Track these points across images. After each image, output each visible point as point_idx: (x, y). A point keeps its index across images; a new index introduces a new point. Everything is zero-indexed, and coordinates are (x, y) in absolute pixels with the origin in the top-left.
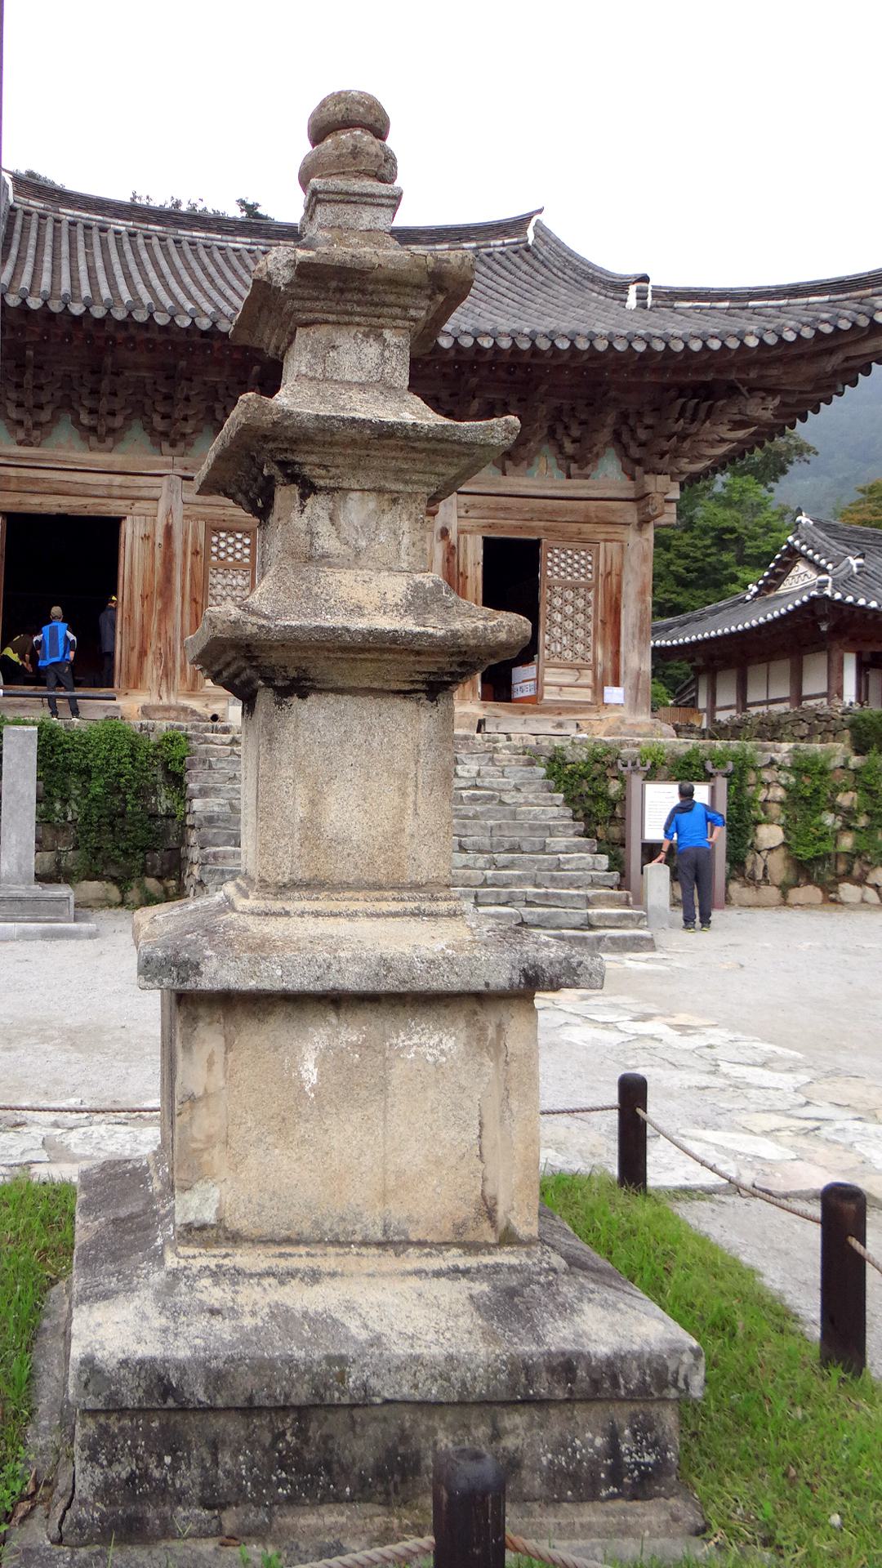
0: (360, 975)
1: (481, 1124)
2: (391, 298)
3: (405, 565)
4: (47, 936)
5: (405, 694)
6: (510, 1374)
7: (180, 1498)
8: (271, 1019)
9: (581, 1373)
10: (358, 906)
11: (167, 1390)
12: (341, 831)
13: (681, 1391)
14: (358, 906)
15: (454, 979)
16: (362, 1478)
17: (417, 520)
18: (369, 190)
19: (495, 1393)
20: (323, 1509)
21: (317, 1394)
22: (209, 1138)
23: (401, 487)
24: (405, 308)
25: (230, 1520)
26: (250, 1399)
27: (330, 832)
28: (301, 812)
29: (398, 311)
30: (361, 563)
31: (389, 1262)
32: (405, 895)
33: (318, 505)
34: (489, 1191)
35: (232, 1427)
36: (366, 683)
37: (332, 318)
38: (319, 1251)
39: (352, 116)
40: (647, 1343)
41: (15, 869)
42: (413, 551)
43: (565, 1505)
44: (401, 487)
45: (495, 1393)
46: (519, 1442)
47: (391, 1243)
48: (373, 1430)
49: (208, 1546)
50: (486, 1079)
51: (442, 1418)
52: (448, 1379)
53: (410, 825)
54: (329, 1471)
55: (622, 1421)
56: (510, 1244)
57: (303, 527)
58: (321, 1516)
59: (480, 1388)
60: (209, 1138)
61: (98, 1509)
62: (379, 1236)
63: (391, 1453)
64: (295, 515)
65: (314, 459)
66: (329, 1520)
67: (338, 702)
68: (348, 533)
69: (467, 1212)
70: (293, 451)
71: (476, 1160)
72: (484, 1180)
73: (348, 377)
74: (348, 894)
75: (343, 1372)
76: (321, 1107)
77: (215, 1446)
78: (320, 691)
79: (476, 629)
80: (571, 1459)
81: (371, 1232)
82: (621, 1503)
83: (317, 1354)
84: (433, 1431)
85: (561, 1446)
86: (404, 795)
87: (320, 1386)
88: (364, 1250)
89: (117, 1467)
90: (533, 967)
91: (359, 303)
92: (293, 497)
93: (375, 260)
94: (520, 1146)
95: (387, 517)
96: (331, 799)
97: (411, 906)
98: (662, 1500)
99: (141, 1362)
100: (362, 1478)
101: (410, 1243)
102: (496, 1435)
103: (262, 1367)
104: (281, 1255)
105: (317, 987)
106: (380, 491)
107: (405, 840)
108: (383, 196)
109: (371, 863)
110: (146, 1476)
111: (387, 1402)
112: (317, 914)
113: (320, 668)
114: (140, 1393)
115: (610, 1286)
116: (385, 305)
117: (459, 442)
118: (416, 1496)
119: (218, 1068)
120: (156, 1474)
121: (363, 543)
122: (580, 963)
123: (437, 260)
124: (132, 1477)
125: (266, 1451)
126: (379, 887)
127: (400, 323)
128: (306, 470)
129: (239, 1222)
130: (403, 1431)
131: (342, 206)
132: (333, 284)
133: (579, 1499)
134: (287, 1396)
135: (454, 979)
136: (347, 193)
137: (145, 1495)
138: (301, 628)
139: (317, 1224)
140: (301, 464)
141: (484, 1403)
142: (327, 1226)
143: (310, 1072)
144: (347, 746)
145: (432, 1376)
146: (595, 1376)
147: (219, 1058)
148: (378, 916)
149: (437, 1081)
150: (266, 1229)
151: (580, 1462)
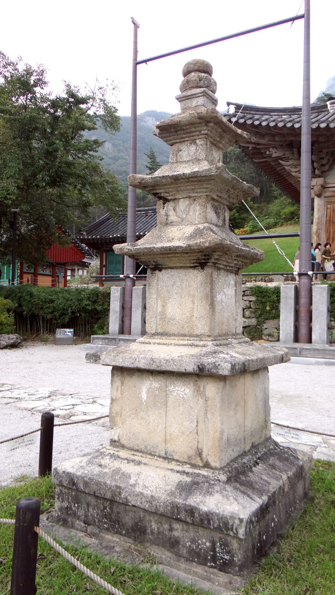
0: (145, 363)
1: (197, 421)
2: (193, 129)
3: (197, 222)
4: (326, 364)
5: (194, 267)
6: (171, 508)
7: (78, 518)
8: (134, 377)
9: (196, 515)
10: (173, 342)
11: (74, 484)
12: (180, 314)
13: (235, 534)
14: (173, 342)
15: (175, 367)
16: (128, 530)
17: (202, 205)
18: (193, 93)
19: (166, 513)
20: (115, 535)
21: (113, 496)
22: (117, 413)
23: (196, 195)
24: (200, 131)
25: (90, 529)
26: (94, 492)
27: (169, 316)
28: (160, 309)
29: (198, 133)
30: (184, 223)
31: (165, 464)
32: (192, 339)
33: (170, 206)
34: (200, 446)
35: (92, 500)
36: (178, 265)
37: (178, 141)
38: (145, 456)
39: (190, 69)
40: (224, 511)
41: (318, 339)
42: (200, 216)
43: (194, 563)
44: (196, 195)
45: (166, 513)
46: (179, 534)
47: (167, 458)
48: (131, 514)
49: (82, 534)
50: (200, 405)
51: (154, 518)
52: (151, 504)
53: (196, 314)
54: (119, 524)
55: (217, 539)
56: (208, 468)
57: (164, 214)
58: (113, 537)
59: (162, 510)
60: (117, 413)
61: (58, 513)
62: (164, 455)
63: (136, 524)
64: (161, 210)
65: (162, 191)
66: (114, 539)
67: (171, 272)
68: (180, 213)
69: (192, 452)
70: (155, 190)
71: (196, 435)
72: (198, 442)
73: (185, 160)
74: (173, 338)
75: (120, 492)
76: (147, 408)
77: (88, 505)
78: (165, 268)
79: (196, 243)
80: (197, 547)
81: (161, 453)
82: (215, 571)
83: (113, 484)
84: (151, 521)
85: (193, 541)
86: (194, 303)
87: (114, 495)
88: (158, 459)
89: (64, 503)
90: (201, 365)
91: (184, 134)
92: (160, 204)
93: (178, 119)
94: (212, 432)
95: (192, 206)
96: (169, 305)
97: (190, 342)
98: (231, 575)
99: (68, 473)
100: (128, 530)
101: (174, 460)
102: (171, 529)
103: (98, 483)
104: (133, 455)
105: (132, 366)
106: (189, 197)
107: (194, 319)
108: (198, 94)
109: (183, 327)
110: (71, 508)
111: (134, 506)
112: (159, 344)
113: (160, 261)
114: (67, 482)
115: (244, 493)
116: (192, 132)
117: (200, 176)
118: (144, 542)
119: (119, 391)
120: (73, 509)
121: (184, 216)
122: (219, 365)
123: (198, 113)
124: (67, 508)
125: (101, 512)
126: (185, 335)
127: (201, 136)
128: (162, 195)
129: (124, 442)
130: (140, 517)
131: (187, 101)
132: (172, 130)
133: (199, 563)
134: (104, 495)
135: (175, 367)
136: (186, 96)
137: (70, 514)
138: (140, 248)
139: (146, 447)
140: (160, 193)
141: (162, 515)
142: (148, 448)
143: (144, 396)
144: (175, 287)
145: (147, 501)
146: (202, 518)
147: (119, 388)
148: (178, 345)
149: (183, 404)
150: (131, 446)
151: (200, 549)
